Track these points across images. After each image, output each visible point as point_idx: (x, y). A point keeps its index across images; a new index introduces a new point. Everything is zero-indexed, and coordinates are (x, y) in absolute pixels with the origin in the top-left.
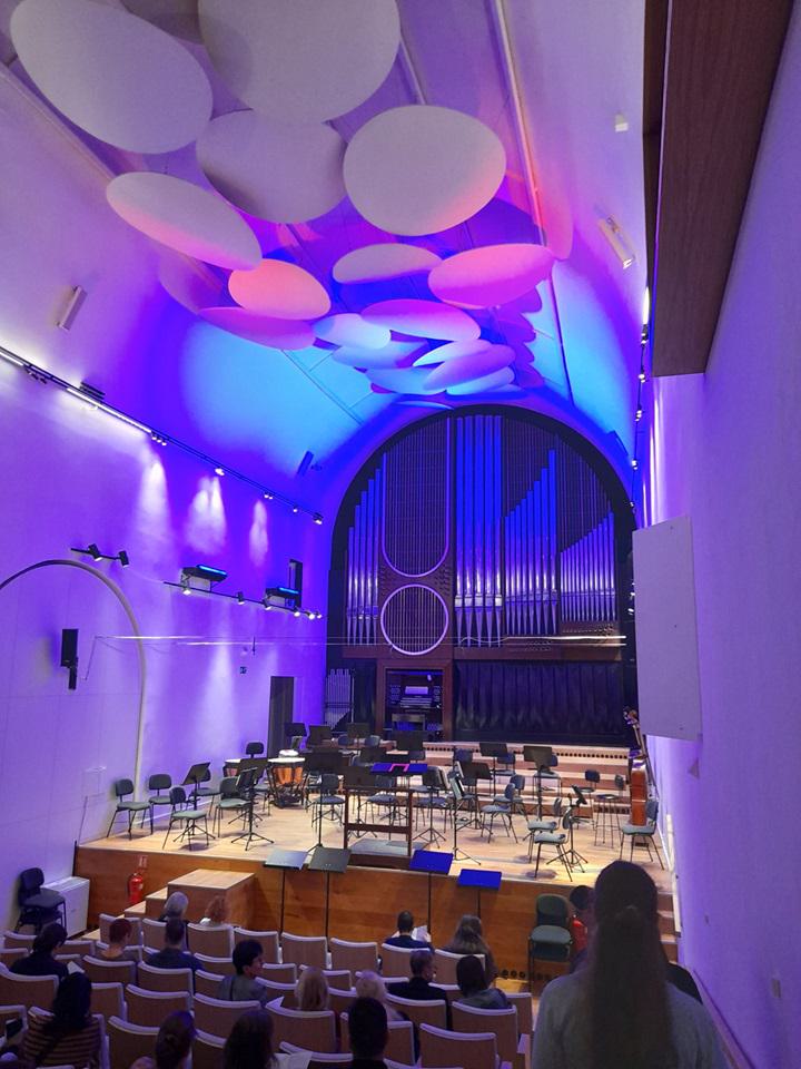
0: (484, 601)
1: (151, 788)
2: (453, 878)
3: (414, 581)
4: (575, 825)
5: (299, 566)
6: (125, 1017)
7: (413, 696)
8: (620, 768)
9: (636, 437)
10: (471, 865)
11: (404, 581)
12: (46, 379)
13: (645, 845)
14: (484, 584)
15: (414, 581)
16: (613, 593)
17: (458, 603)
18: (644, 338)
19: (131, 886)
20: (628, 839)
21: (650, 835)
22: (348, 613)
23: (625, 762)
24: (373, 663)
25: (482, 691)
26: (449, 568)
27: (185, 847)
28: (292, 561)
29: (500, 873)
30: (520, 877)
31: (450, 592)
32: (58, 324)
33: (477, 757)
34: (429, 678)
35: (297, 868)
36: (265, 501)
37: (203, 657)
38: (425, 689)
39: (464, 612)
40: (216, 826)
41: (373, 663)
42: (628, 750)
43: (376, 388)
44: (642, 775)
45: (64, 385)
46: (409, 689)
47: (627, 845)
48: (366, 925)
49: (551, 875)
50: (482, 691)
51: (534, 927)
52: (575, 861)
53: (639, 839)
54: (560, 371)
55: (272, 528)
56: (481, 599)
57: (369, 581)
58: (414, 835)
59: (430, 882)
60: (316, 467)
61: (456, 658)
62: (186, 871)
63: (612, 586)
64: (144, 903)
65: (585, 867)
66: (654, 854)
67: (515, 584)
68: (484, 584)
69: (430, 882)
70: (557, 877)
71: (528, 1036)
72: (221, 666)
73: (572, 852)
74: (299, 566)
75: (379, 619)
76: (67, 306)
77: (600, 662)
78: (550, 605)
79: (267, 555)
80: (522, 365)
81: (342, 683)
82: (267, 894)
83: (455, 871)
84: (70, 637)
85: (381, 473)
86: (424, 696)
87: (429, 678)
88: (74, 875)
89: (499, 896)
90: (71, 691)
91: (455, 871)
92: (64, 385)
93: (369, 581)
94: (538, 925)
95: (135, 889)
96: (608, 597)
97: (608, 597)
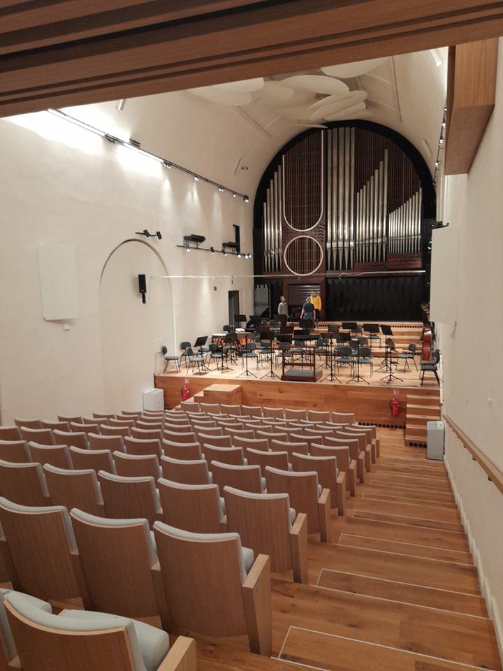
0: (344, 244)
1: (182, 348)
3: (303, 233)
4: (225, 359)
6: (115, 471)
8: (417, 333)
11: (298, 234)
12: (111, 140)
14: (344, 228)
15: (303, 233)
16: (420, 237)
17: (329, 245)
19: (182, 392)
22: (265, 253)
23: (421, 330)
26: (323, 225)
27: (195, 374)
31: (324, 240)
32: (117, 107)
33: (341, 330)
37: (198, 283)
40: (245, 361)
42: (421, 323)
44: (429, 336)
45: (121, 142)
56: (342, 243)
57: (277, 230)
58: (316, 367)
62: (208, 385)
63: (419, 232)
64: (203, 392)
67: (362, 228)
68: (344, 228)
71: (355, 461)
72: (206, 289)
75: (283, 256)
78: (382, 245)
82: (247, 393)
84: (142, 279)
88: (155, 387)
90: (144, 305)
92: (121, 142)
93: (277, 230)
95: (186, 393)
96: (416, 240)
97: (416, 240)
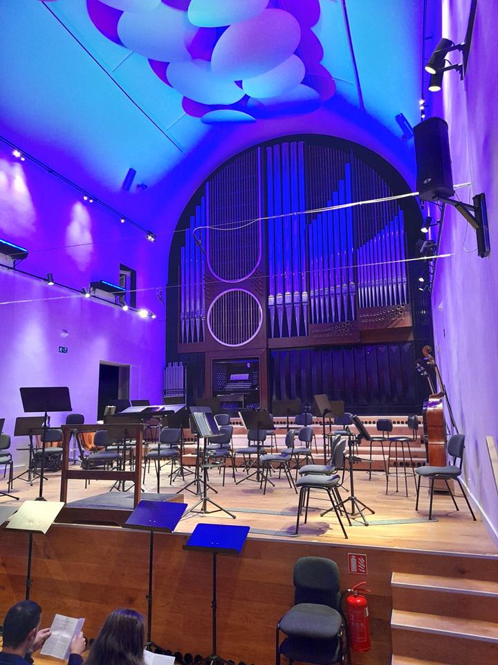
2: (183, 536)
5: (134, 274)
7: (236, 381)
9: (423, 84)
10: (216, 518)
13: (447, 492)
18: (422, 372)
20: (426, 482)
21: (455, 476)
24: (201, 356)
25: (293, 379)
28: (123, 268)
29: (248, 528)
30: (276, 534)
34: (249, 365)
35: (40, 532)
36: (85, 204)
38: (246, 376)
39: (276, 308)
41: (201, 356)
43: (193, 107)
44: (440, 414)
46: (233, 377)
47: (424, 491)
48: (81, 599)
49: (322, 529)
50: (293, 379)
51: (292, 606)
52: (356, 511)
53: (439, 484)
54: (354, 81)
55: (97, 230)
59: (297, 531)
60: (142, 187)
61: (270, 347)
65: (369, 518)
66: (461, 502)
69: (297, 531)
70: (328, 532)
73: (353, 500)
74: (134, 274)
76: (273, 386)
77: (394, 343)
79: (93, 254)
80: (316, 75)
81: (177, 376)
83: (186, 526)
85: (205, 199)
86: (245, 381)
87: (249, 365)
89: (246, 560)
91: (186, 526)
94: (296, 604)
